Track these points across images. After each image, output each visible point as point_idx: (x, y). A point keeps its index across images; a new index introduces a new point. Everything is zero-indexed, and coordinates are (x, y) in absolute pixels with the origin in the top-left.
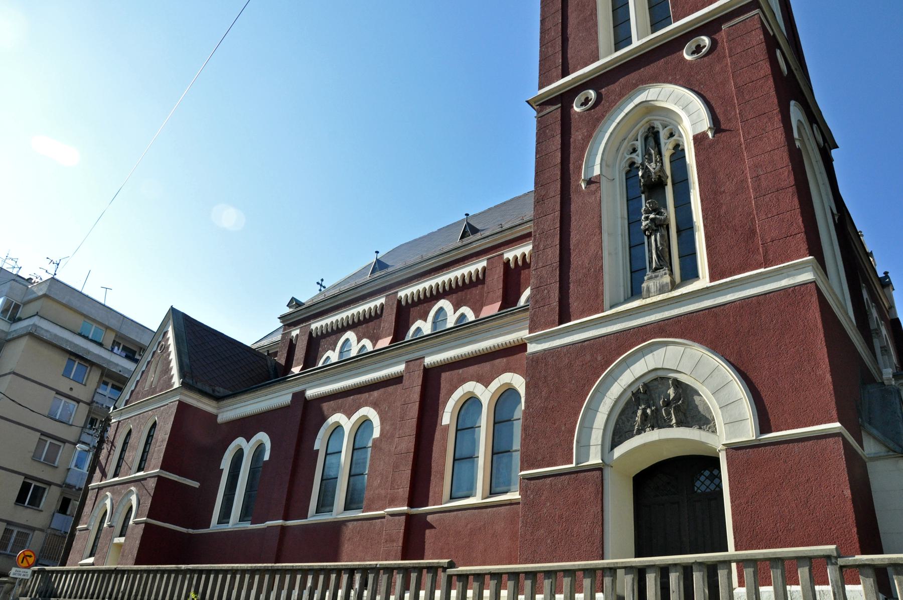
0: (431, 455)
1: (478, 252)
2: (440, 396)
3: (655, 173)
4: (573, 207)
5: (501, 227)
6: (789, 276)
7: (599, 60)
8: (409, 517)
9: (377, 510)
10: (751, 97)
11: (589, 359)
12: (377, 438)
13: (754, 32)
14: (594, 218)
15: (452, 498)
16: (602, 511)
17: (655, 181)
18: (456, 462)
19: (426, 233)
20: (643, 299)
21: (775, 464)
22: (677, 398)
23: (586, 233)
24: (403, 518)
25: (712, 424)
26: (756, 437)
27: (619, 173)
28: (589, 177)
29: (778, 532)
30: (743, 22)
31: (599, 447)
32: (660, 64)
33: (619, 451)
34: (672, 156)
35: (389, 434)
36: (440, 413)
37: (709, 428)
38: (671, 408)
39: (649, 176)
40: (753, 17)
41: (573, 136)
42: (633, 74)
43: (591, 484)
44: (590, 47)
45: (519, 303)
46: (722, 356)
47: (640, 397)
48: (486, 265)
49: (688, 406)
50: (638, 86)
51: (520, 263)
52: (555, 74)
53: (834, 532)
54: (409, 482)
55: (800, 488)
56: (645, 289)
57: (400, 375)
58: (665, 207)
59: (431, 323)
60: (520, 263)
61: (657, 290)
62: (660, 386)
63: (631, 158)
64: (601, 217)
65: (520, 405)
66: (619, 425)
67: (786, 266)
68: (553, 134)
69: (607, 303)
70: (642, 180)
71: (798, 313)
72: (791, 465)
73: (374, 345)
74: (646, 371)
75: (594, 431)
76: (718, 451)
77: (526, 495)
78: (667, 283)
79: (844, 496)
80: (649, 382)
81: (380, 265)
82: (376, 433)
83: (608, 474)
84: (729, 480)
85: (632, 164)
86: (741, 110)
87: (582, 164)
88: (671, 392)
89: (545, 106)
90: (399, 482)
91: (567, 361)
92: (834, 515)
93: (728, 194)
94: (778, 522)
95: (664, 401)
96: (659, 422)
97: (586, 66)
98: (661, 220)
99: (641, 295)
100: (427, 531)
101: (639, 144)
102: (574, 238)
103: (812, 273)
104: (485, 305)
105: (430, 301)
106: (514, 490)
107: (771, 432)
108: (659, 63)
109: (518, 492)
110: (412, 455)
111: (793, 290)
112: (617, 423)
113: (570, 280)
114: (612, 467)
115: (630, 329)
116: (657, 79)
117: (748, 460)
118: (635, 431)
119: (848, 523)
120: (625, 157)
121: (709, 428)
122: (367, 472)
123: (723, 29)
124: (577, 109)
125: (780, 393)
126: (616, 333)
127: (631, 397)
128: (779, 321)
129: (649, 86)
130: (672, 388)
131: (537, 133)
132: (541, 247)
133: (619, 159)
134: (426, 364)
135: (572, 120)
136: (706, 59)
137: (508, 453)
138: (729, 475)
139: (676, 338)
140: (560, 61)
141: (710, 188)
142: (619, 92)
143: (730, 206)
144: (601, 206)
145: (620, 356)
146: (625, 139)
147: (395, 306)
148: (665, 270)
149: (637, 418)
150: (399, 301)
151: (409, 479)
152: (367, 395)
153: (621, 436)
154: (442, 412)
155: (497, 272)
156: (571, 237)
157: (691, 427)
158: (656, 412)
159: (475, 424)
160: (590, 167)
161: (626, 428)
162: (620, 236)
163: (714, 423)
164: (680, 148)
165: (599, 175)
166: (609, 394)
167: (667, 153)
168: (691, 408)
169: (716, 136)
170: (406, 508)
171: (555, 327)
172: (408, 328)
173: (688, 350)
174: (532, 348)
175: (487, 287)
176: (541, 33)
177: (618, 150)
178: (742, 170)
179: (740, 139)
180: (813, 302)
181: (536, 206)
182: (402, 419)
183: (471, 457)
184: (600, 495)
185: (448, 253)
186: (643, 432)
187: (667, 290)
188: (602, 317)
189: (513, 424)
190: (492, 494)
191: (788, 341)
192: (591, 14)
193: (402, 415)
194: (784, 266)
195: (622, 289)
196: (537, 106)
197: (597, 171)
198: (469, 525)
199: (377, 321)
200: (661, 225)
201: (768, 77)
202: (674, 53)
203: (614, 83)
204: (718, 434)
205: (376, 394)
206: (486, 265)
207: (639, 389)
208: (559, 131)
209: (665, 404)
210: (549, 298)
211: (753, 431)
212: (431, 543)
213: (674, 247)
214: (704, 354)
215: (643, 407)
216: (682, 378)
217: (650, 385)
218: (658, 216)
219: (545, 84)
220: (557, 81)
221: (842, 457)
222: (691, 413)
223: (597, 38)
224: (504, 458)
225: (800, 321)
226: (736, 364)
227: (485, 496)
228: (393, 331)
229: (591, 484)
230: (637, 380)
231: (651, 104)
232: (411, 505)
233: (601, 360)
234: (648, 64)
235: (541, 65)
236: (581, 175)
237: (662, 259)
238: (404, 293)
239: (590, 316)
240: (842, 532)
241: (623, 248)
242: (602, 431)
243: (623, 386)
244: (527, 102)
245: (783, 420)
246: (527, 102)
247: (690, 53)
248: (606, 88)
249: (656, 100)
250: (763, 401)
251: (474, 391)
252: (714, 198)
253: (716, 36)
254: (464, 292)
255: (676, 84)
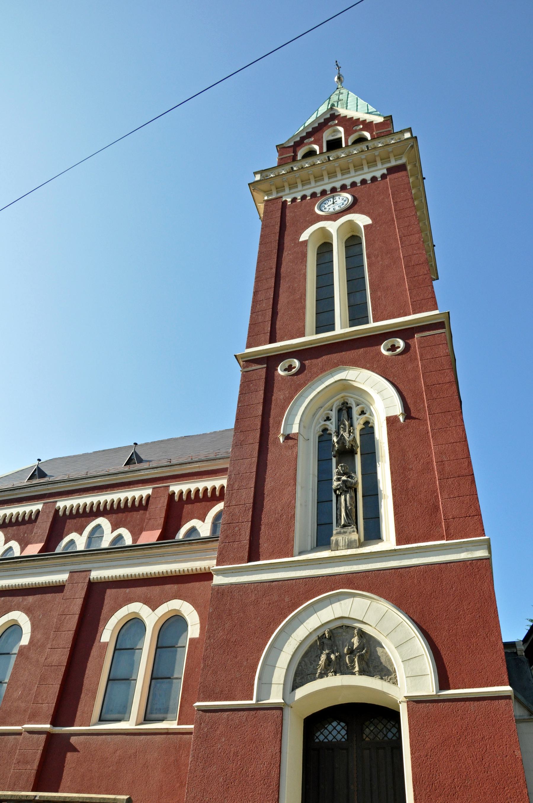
0: (85, 671)
1: (145, 479)
2: (103, 612)
3: (349, 442)
4: (270, 457)
5: (170, 462)
6: (467, 551)
7: (304, 336)
8: (50, 737)
9: (12, 725)
10: (438, 396)
11: (276, 599)
12: (25, 646)
13: (441, 346)
14: (289, 470)
15: (102, 720)
16: (280, 752)
17: (348, 448)
18: (110, 682)
19: (81, 453)
20: (332, 551)
21: (453, 719)
22: (361, 647)
23: (281, 482)
24: (44, 736)
25: (393, 676)
26: (437, 693)
27: (314, 435)
28: (288, 433)
29: (455, 787)
30: (433, 336)
31: (281, 686)
32: (360, 352)
33: (301, 692)
34: (362, 430)
35: (39, 644)
36: (100, 629)
37: (390, 679)
38: (355, 656)
39: (343, 443)
40: (441, 334)
41: (274, 395)
42: (335, 355)
43: (270, 723)
44: (298, 324)
45: (178, 534)
46: (406, 613)
47: (324, 642)
48: (151, 494)
49: (371, 655)
50: (339, 365)
51: (184, 497)
52: (263, 339)
53: (507, 792)
54: (56, 697)
55: (476, 745)
56: (334, 542)
57: (62, 584)
58: (355, 473)
59: (86, 537)
60: (184, 497)
61: (345, 545)
62: (344, 634)
63: (325, 425)
64: (296, 470)
65: (186, 633)
66: (301, 666)
67: (466, 541)
68: (257, 389)
69: (296, 549)
70: (337, 445)
71: (475, 584)
72: (468, 722)
73: (22, 550)
74: (333, 618)
75: (276, 669)
76: (398, 702)
77: (200, 727)
78: (355, 540)
79: (516, 756)
80: (334, 629)
81: (39, 473)
82: (25, 640)
83: (288, 714)
84: (410, 732)
85: (325, 430)
86: (429, 405)
87: (282, 421)
88: (356, 641)
89: (251, 364)
90: (44, 696)
91: (253, 598)
92: (507, 775)
93: (415, 472)
94: (456, 777)
95: (348, 649)
96: (342, 668)
97: (292, 339)
98: (352, 483)
99: (330, 547)
100: (69, 755)
101: (333, 415)
102: (269, 484)
103: (487, 551)
104: (144, 530)
105: (89, 517)
106: (170, 719)
107: (449, 689)
108: (359, 352)
109: (177, 721)
110: (63, 669)
111: (470, 564)
112: (300, 664)
113: (262, 522)
114: (292, 707)
115: (320, 577)
116: (356, 363)
117: (428, 714)
118: (317, 675)
119: (519, 784)
120: (320, 423)
121: (390, 679)
122: (7, 680)
123: (416, 337)
124: (280, 372)
125: (458, 654)
126: (305, 578)
127: (316, 641)
128: (458, 588)
129: (349, 368)
130: (356, 638)
131: (241, 384)
132: (236, 487)
133: (314, 424)
134: (91, 577)
135: (276, 381)
136: (400, 357)
137: (168, 680)
138: (410, 727)
139: (363, 591)
140: (269, 329)
141: (400, 464)
142: (321, 366)
143: (417, 482)
144: (297, 461)
145: (308, 601)
146: (321, 407)
147: (52, 515)
148: (353, 528)
149: (320, 662)
150: (57, 511)
151: (57, 694)
152: (20, 599)
153: (303, 678)
154: (102, 629)
155: (161, 502)
156: (266, 483)
157: (373, 677)
158: (340, 658)
159: (136, 645)
160: (289, 424)
161: (308, 671)
162: (311, 490)
163: (395, 675)
164: (370, 425)
165: (298, 433)
166: (294, 635)
167: (358, 425)
168: (373, 658)
169: (406, 421)
170: (48, 726)
171: (244, 563)
172: (62, 539)
173: (374, 604)
174: (217, 580)
175: (150, 514)
176: (253, 302)
177: (314, 415)
178: (428, 454)
179: (427, 428)
180: (488, 576)
181: (234, 448)
182: (58, 630)
183: (128, 679)
184: (279, 736)
185: (115, 475)
186: (325, 676)
187: (355, 546)
188: (286, 562)
189: (176, 651)
190: (147, 719)
191: (465, 608)
192: (301, 298)
193: (58, 626)
194: (464, 542)
195: (310, 538)
196: (243, 361)
197: (295, 429)
198: (118, 752)
199: (30, 526)
200: (350, 488)
201: (453, 384)
202: (372, 346)
203: (317, 358)
204: (399, 685)
205: (30, 599)
206: (151, 494)
207: (324, 634)
208: (262, 388)
209: (349, 652)
210: (240, 535)
211: (433, 686)
212: (71, 768)
213: (360, 509)
214: (389, 609)
215: (327, 652)
216: (366, 629)
217: (334, 632)
218: (350, 480)
219: (253, 345)
220: (265, 345)
221: (513, 719)
222: (374, 663)
223: (305, 318)
224: (164, 685)
225: (477, 591)
226: (418, 623)
227: (138, 722)
228: (45, 539)
229: (270, 723)
230: (323, 625)
231: (349, 383)
232: (54, 723)
233: (288, 602)
234: (350, 350)
235: (250, 328)
236: (280, 430)
237: (350, 517)
238: (63, 504)
239: (279, 558)
240: (514, 793)
241: (312, 501)
242: (285, 670)
243: (309, 629)
244: (235, 356)
245: (461, 679)
246: (235, 356)
247: (386, 349)
248: (310, 361)
249: (354, 381)
250: (442, 659)
251: (139, 613)
252: (403, 473)
253: (410, 341)
254: (124, 515)
255: (373, 371)
